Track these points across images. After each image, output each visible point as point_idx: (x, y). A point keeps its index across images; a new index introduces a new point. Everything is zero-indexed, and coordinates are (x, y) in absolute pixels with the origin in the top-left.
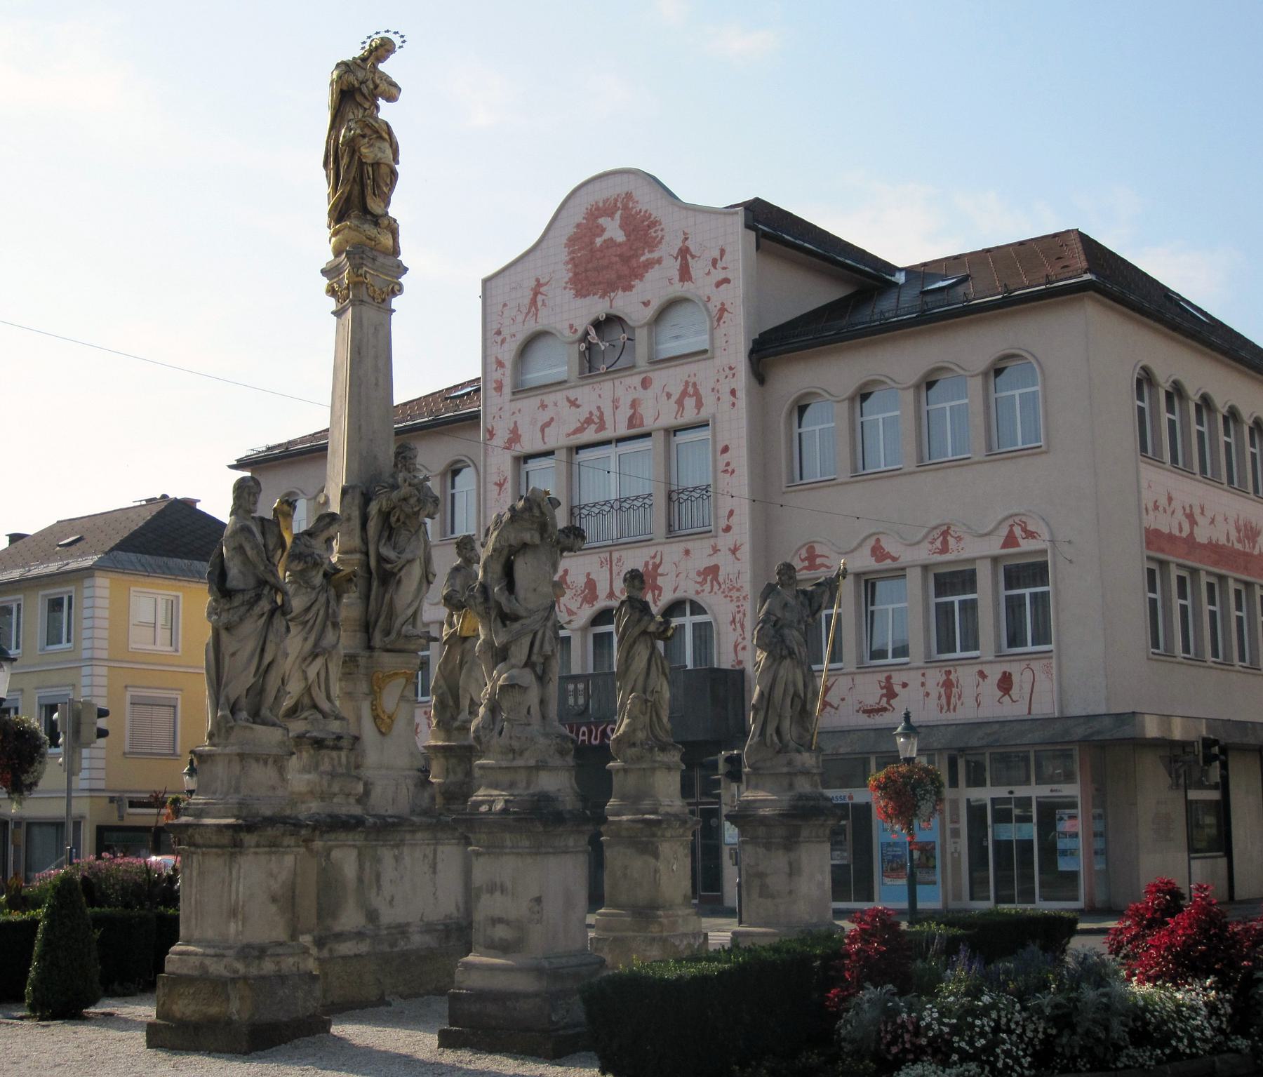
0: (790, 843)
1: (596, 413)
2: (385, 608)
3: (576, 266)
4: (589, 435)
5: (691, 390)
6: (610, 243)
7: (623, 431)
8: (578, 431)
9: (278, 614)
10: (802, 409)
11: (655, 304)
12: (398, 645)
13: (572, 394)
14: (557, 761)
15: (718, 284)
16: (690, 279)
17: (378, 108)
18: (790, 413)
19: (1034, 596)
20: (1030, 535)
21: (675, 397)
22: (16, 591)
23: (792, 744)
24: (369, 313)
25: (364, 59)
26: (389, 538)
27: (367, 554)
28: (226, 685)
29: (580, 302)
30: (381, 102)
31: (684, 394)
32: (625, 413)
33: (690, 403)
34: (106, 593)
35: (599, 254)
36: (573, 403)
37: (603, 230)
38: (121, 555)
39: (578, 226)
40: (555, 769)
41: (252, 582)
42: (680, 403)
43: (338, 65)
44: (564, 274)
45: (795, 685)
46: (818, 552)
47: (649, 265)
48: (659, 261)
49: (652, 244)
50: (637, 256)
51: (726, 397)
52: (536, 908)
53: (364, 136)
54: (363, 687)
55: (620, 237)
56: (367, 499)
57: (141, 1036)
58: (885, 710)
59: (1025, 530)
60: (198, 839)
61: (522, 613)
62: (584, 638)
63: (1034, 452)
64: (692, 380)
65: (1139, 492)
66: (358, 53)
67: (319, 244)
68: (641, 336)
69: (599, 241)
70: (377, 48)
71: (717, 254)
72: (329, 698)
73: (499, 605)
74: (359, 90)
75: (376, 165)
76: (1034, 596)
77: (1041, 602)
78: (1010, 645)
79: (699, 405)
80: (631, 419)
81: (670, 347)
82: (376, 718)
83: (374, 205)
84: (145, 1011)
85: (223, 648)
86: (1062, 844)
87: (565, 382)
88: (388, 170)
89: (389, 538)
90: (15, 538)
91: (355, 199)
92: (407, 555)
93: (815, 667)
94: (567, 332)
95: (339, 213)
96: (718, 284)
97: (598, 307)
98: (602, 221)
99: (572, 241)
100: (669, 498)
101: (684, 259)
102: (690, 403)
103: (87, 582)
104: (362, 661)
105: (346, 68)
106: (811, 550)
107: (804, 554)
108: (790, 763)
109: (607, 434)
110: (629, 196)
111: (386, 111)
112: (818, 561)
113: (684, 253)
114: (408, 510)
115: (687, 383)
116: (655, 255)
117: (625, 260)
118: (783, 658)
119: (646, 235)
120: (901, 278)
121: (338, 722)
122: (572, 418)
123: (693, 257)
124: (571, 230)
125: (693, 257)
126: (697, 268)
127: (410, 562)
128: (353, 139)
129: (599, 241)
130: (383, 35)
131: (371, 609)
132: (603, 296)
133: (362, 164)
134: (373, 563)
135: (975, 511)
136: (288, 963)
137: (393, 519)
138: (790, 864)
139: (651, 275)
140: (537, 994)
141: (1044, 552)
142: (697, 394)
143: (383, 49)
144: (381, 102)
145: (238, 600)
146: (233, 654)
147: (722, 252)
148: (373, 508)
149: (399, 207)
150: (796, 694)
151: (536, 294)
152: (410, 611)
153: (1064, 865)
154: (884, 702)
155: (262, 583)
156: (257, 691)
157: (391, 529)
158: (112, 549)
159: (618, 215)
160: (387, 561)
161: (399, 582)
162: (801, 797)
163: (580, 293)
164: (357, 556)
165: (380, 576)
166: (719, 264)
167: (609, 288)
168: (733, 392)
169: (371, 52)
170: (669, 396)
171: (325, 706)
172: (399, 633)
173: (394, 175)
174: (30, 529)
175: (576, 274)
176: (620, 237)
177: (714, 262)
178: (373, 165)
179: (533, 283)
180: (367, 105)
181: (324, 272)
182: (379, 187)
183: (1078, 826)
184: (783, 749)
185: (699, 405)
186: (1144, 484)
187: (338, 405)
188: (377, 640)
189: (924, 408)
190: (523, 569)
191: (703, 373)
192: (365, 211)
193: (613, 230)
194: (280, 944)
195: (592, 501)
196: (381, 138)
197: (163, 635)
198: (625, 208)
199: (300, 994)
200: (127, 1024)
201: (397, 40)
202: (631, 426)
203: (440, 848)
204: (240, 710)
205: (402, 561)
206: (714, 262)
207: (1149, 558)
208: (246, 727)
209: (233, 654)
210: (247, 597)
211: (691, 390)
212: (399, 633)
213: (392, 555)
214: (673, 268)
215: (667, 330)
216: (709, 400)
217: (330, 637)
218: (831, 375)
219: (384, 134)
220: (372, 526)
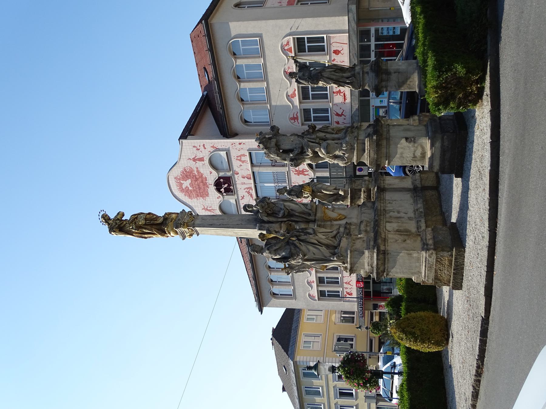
0: (388, 73)
1: (246, 190)
2: (301, 215)
3: (198, 196)
5: (239, 158)
6: (191, 184)
7: (252, 181)
9: (300, 238)
10: (246, 121)
11: (211, 170)
12: (314, 211)
13: (240, 198)
14: (356, 134)
15: (205, 148)
16: (203, 158)
17: (126, 220)
18: (247, 125)
19: (308, 42)
20: (288, 43)
21: (241, 163)
22: (300, 387)
23: (353, 73)
24: (197, 222)
25: (109, 224)
26: (276, 214)
27: (282, 222)
28: (325, 257)
29: (209, 195)
30: (124, 219)
31: (240, 160)
33: (243, 158)
34: (302, 357)
35: (195, 188)
36: (243, 198)
37: (187, 187)
38: (289, 353)
40: (358, 134)
41: (288, 247)
42: (243, 162)
43: (110, 233)
45: (331, 72)
46: (292, 116)
47: (198, 171)
49: (191, 171)
50: (195, 176)
51: (242, 146)
52: (410, 140)
53: (135, 223)
54: (329, 223)
56: (263, 222)
57: (456, 293)
58: (344, 94)
59: (286, 45)
60: (382, 269)
61: (301, 146)
62: (318, 172)
63: (261, 41)
64: (236, 158)
65: (275, 7)
66: (107, 226)
67: (172, 241)
68: (222, 174)
69: (190, 188)
70: (105, 220)
71: (195, 149)
72: (332, 232)
73: (298, 154)
74: (118, 225)
75: (146, 219)
76: (308, 42)
77: (310, 40)
78: (324, 51)
79: (244, 155)
80: (248, 178)
81: (225, 165)
82: (340, 219)
83: (161, 220)
84: (446, 290)
85: (312, 258)
86: (391, 33)
87: (236, 200)
88: (148, 216)
89: (276, 214)
90: (284, 390)
91: (158, 227)
92: (283, 207)
93: (327, 65)
94: (220, 200)
95: (163, 233)
96: (205, 148)
97: (212, 189)
98: (184, 187)
99: (190, 197)
100: (274, 166)
101: (196, 160)
102: (243, 158)
103: (298, 363)
104: (319, 223)
105: (112, 230)
106: (291, 119)
107: (293, 121)
108: (359, 73)
109: (253, 186)
110: (175, 178)
111: (127, 217)
112: (295, 116)
113: (194, 160)
114: (266, 207)
115: (237, 159)
116: (195, 169)
117: (197, 180)
118: (321, 75)
119: (188, 172)
120: (206, 93)
121: (341, 229)
123: (196, 157)
124: (187, 197)
125: (196, 157)
126: (200, 155)
127: (284, 206)
128: (136, 227)
129: (190, 188)
130: (100, 217)
131: (300, 220)
132: (208, 187)
133: (145, 224)
134: (285, 219)
135: (279, 64)
136: (429, 236)
137: (270, 212)
138: (395, 72)
139: (202, 170)
140: (442, 139)
141: (294, 38)
143: (106, 218)
144: (124, 219)
145: (293, 251)
146: (314, 254)
147: (194, 147)
148: (266, 219)
149: (160, 213)
150: (334, 71)
151: (207, 210)
152: (302, 206)
153: (398, 32)
154: (342, 94)
155: (288, 243)
156: (328, 246)
157: (273, 213)
158: (287, 353)
159: (182, 182)
160: (284, 214)
161: (292, 210)
162: (371, 69)
164: (282, 224)
165: (290, 215)
166: (198, 148)
167: (205, 185)
168: (240, 144)
169: (106, 222)
170: (241, 166)
171: (335, 232)
172: (310, 210)
173: (149, 214)
174: (281, 384)
175: (201, 196)
176: (189, 181)
178: (146, 221)
179: (204, 210)
180: (125, 223)
181: (184, 239)
182: (154, 218)
183: (385, 27)
184: (354, 75)
185: (244, 155)
186: (273, 6)
187: (229, 233)
188: (312, 218)
189: (250, 102)
190: (286, 145)
191: (234, 154)
192: (162, 224)
193: (187, 183)
194: (422, 239)
195: (272, 178)
196: (136, 218)
197: (317, 339)
198: (179, 179)
199: (441, 232)
200: (451, 295)
201: (102, 213)
202: (250, 178)
203: (387, 199)
204: (334, 252)
205: (285, 209)
207: (297, 4)
208: (341, 249)
209: (314, 254)
210: (293, 248)
211: (239, 158)
212: (310, 210)
213: (282, 212)
214: (199, 164)
215: (219, 166)
216: (242, 152)
217: (310, 231)
218: (235, 110)
219: (135, 217)
220: (271, 219)
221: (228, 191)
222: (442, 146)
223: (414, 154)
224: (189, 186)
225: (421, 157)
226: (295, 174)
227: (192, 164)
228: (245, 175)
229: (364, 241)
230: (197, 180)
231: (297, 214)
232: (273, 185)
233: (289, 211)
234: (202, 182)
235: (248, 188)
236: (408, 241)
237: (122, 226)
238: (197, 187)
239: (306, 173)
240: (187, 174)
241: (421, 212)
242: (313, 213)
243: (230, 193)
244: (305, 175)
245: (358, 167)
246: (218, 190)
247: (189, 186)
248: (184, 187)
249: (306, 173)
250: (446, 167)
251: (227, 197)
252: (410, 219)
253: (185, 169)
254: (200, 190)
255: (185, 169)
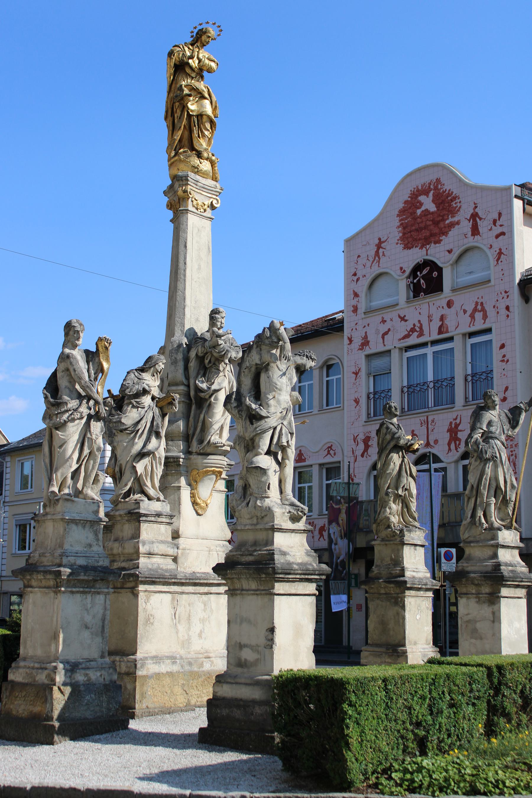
1: (418, 325)
2: (200, 424)
3: (404, 228)
4: (414, 340)
5: (479, 307)
7: (435, 336)
8: (404, 338)
15: (497, 237)
16: (478, 233)
21: (468, 313)
27: (188, 386)
29: (406, 252)
31: (475, 310)
32: (436, 324)
33: (479, 316)
35: (419, 220)
39: (406, 202)
42: (472, 316)
44: (396, 234)
47: (452, 225)
48: (458, 223)
49: (453, 212)
50: (444, 220)
51: (503, 312)
55: (432, 208)
62: (456, 469)
64: (480, 301)
69: (419, 212)
79: (485, 317)
80: (440, 328)
96: (497, 237)
97: (416, 255)
98: (422, 198)
99: (402, 212)
102: (479, 316)
109: (425, 339)
110: (438, 181)
113: (474, 216)
115: (477, 303)
116: (456, 219)
117: (436, 223)
119: (450, 206)
122: (402, 328)
123: (480, 219)
125: (480, 219)
126: (483, 226)
129: (419, 212)
132: (421, 248)
134: (192, 393)
137: (207, 361)
138: (493, 613)
139: (453, 233)
142: (483, 310)
147: (500, 214)
160: (201, 390)
161: (210, 405)
163: (407, 247)
166: (498, 223)
167: (426, 242)
168: (507, 308)
170: (465, 312)
175: (404, 234)
176: (432, 208)
177: (495, 222)
178: (197, 116)
179: (377, 241)
185: (485, 317)
193: (428, 203)
198: (436, 188)
201: (212, 32)
202: (440, 332)
206: (495, 222)
211: (479, 307)
214: (466, 226)
215: (463, 267)
221: (416, 291)
222: (254, 702)
223: (246, 646)
224: (423, 208)
225: (240, 659)
226: (451, 423)
227: (465, 212)
228: (447, 322)
229: (90, 546)
230: (436, 223)
231: (202, 416)
232: (430, 377)
233: (206, 400)
234: (432, 235)
235: (421, 328)
236: (86, 634)
237: (188, 70)
238: (422, 225)
239: (453, 446)
240: (446, 202)
241: (202, 665)
242: (203, 448)
243: (412, 294)
244: (449, 444)
245: (454, 551)
246: (418, 268)
247: (423, 208)
248: (422, 198)
249: (453, 446)
250: (219, 711)
251: (403, 285)
252: (186, 643)
253: (455, 198)
254: (417, 230)
255: (455, 198)
